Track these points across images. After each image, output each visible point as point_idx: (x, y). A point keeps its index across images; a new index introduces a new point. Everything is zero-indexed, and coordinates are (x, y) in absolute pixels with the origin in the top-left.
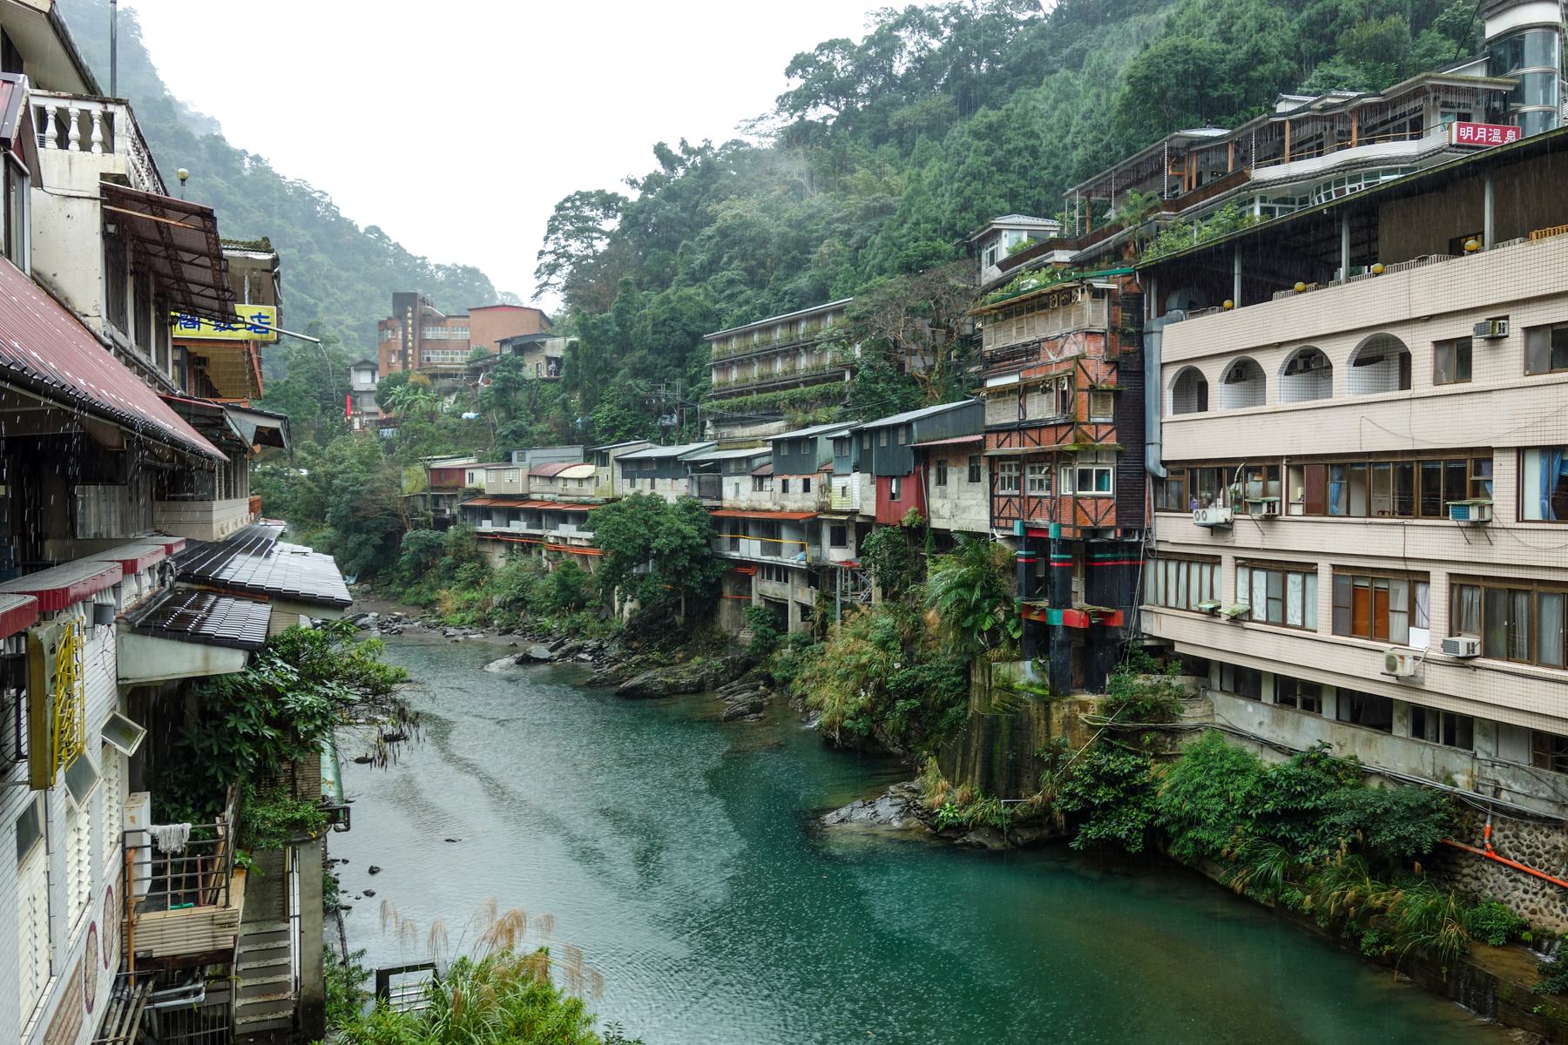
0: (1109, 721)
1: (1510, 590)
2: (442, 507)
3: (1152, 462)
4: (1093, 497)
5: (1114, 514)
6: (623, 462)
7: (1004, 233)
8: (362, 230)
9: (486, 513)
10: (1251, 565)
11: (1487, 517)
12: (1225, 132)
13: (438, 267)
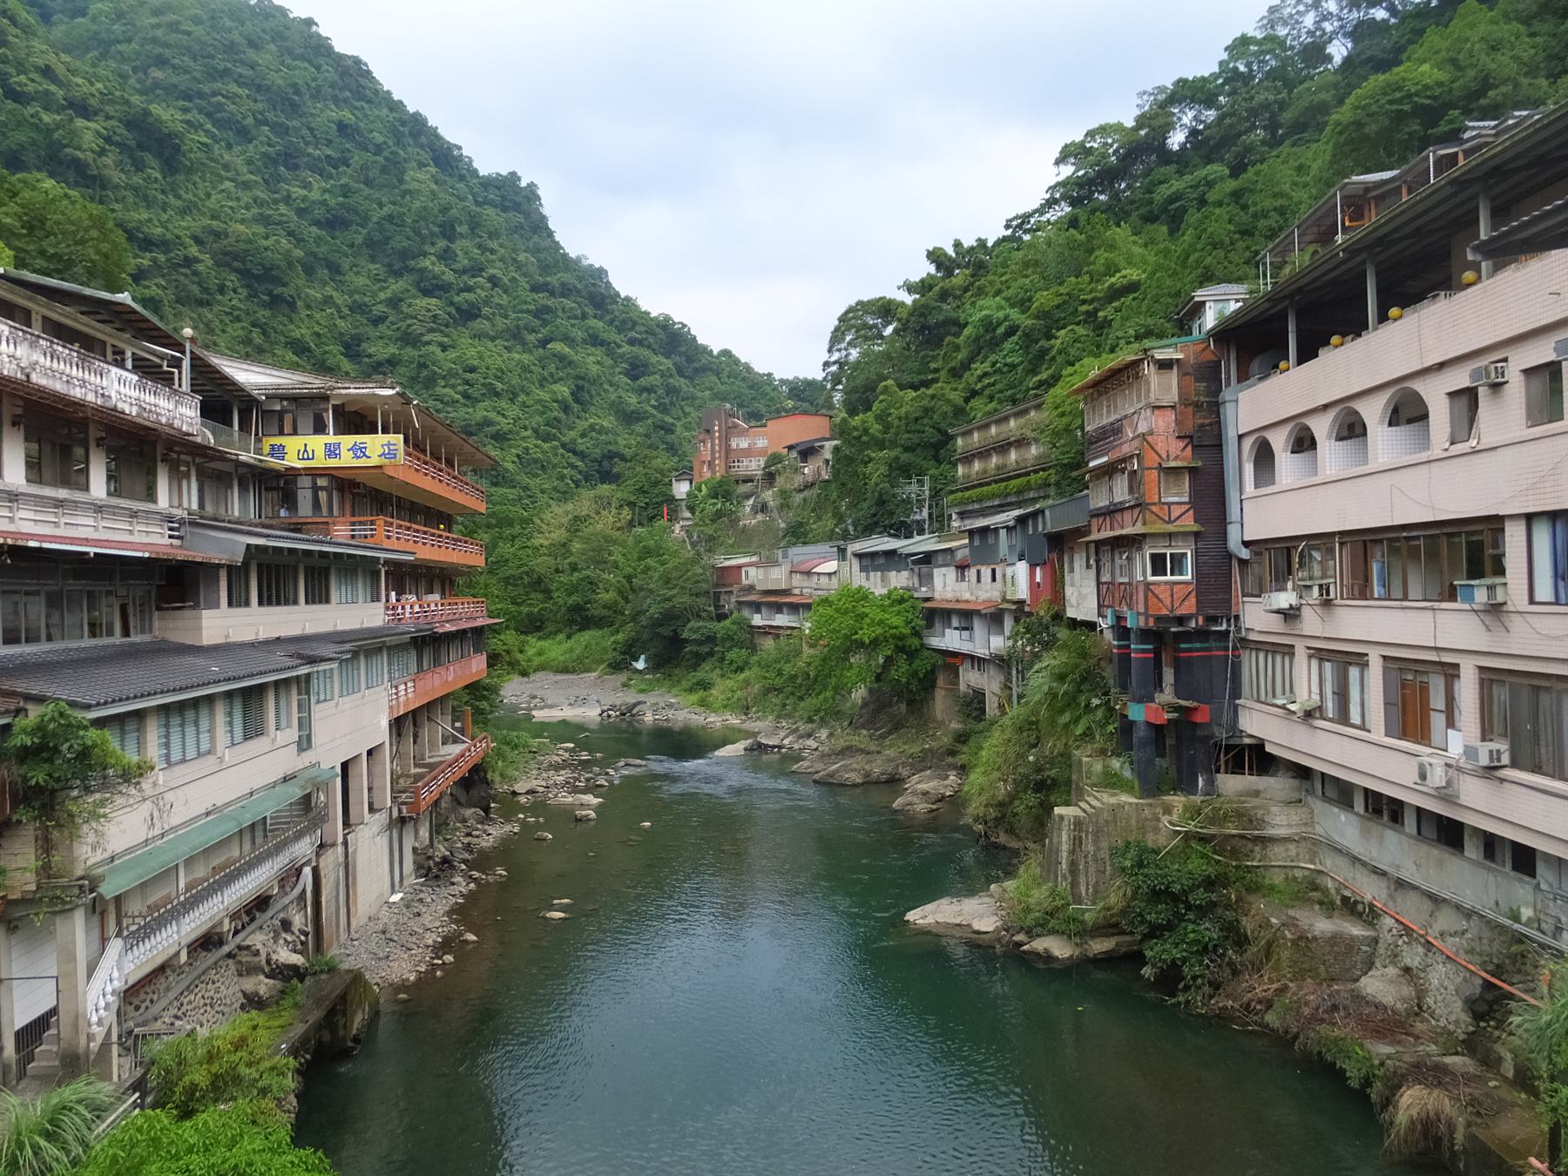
0: (1191, 826)
1: (1533, 686)
2: (722, 603)
3: (1234, 543)
4: (1166, 583)
5: (1194, 600)
6: (860, 556)
7: (1208, 305)
8: (715, 353)
9: (757, 607)
10: (1320, 655)
11: (1500, 599)
12: (1395, 172)
13: (782, 381)
